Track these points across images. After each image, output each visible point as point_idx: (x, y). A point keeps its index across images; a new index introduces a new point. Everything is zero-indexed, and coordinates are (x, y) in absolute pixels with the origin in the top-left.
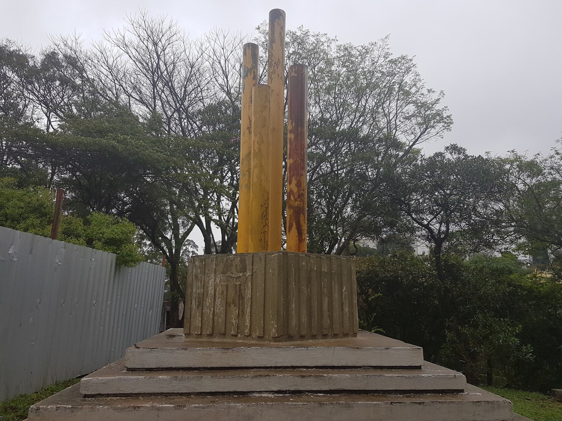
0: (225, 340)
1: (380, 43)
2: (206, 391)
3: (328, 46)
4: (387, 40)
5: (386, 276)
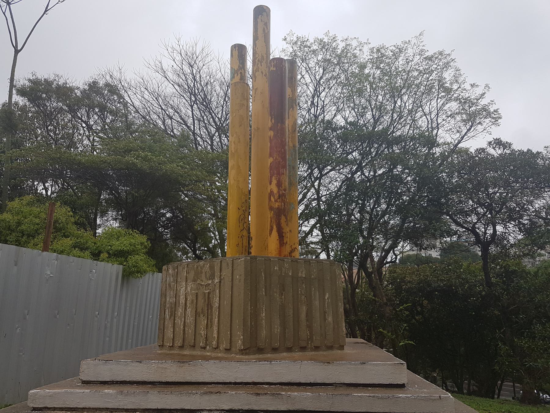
0: (194, 353)
1: (414, 41)
2: (152, 408)
3: (360, 50)
4: (422, 37)
5: (439, 286)
